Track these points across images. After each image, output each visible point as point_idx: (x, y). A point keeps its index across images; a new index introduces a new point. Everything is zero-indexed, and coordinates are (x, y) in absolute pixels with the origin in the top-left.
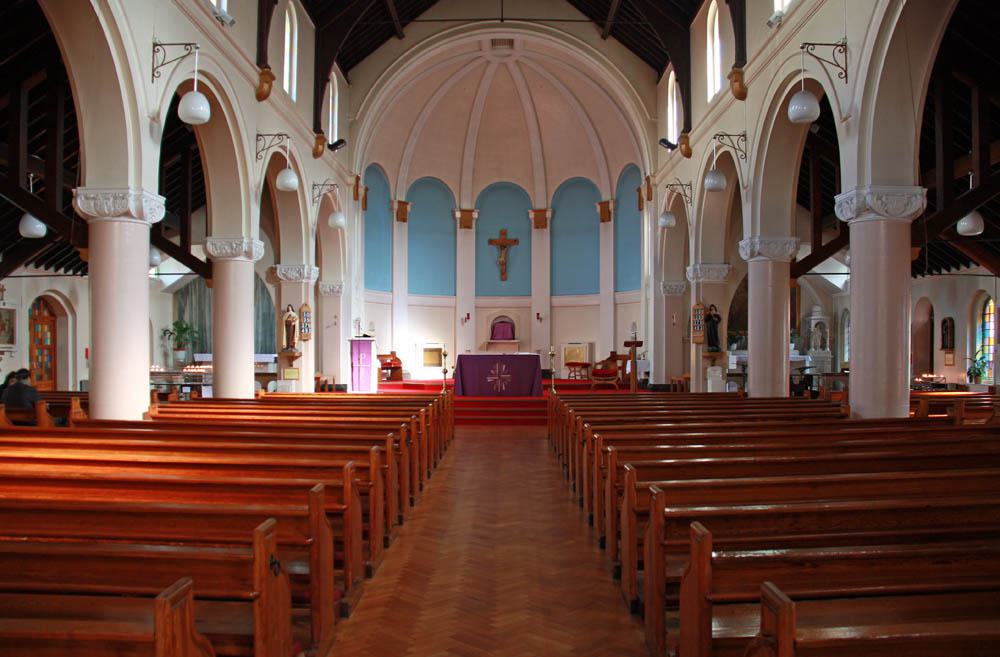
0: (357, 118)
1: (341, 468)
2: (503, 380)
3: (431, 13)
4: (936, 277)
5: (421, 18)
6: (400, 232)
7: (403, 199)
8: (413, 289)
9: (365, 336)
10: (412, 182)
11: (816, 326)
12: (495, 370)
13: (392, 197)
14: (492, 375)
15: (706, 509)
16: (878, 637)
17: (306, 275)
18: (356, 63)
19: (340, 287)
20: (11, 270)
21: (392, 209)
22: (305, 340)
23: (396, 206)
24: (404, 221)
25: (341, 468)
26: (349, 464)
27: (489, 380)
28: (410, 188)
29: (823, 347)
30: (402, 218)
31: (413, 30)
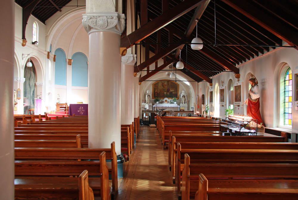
0: (48, 34)
1: (75, 136)
2: (82, 111)
3: (69, 4)
4: (201, 82)
5: (67, 5)
6: (69, 69)
7: (71, 58)
8: (74, 83)
9: (40, 98)
10: (73, 54)
11: (183, 97)
12: (80, 109)
13: (67, 58)
14: (79, 110)
15: (42, 148)
16: (65, 188)
17: (19, 80)
18: (47, 19)
19: (42, 84)
20: (146, 79)
21: (66, 61)
22: (19, 99)
23: (68, 61)
24: (70, 65)
25: (75, 136)
26: (78, 135)
27: (78, 111)
28: (72, 56)
29: (185, 103)
30: (70, 64)
31: (64, 9)
